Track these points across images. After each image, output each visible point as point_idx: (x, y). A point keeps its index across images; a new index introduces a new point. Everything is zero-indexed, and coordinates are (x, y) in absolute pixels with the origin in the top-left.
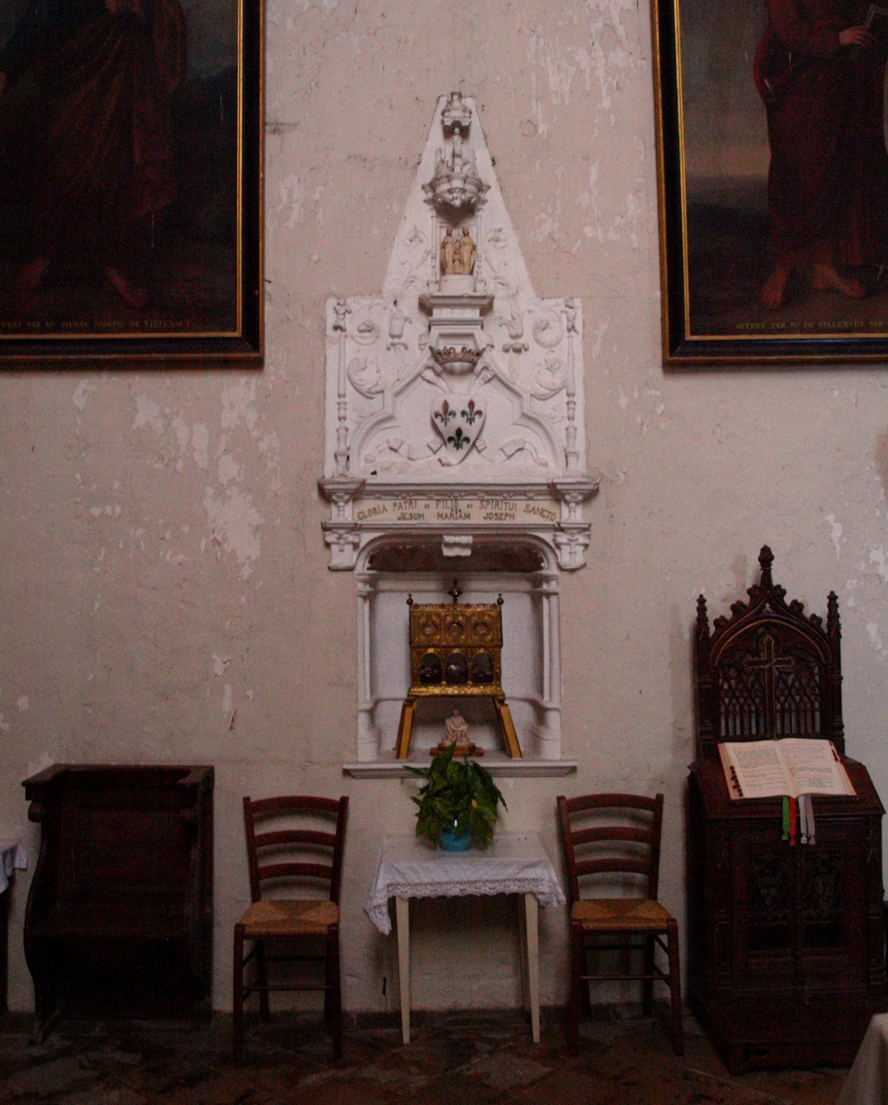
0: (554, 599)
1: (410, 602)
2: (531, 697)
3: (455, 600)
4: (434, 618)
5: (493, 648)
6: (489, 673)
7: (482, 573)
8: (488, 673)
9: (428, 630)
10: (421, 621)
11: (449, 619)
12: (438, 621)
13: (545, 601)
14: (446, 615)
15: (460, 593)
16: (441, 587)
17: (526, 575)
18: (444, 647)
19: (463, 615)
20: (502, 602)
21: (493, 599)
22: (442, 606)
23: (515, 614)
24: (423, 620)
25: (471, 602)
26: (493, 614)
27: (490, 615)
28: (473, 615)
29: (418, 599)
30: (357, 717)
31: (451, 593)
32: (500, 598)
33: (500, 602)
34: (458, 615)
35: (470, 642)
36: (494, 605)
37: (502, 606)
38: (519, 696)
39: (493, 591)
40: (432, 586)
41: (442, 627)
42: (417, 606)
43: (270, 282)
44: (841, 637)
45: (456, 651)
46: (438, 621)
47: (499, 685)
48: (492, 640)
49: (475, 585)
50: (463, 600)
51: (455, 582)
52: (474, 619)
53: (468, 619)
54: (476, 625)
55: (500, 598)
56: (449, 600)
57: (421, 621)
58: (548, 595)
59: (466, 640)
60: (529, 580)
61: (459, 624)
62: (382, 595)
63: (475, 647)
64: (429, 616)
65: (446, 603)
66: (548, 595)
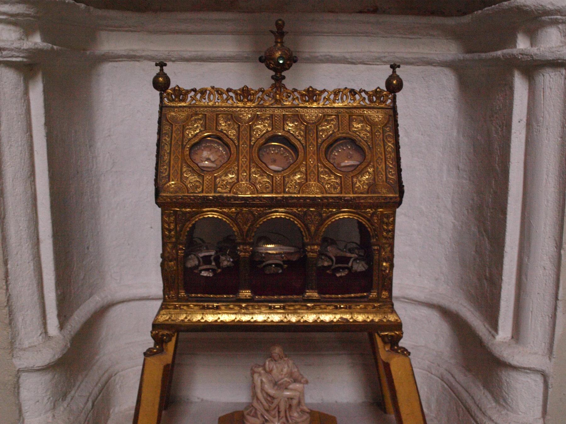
0: (551, 82)
1: (161, 84)
2: (445, 303)
3: (278, 79)
4: (223, 125)
5: (375, 206)
6: (356, 260)
7: (343, 17)
8: (360, 267)
9: (207, 158)
10: (190, 134)
11: (261, 127)
12: (232, 133)
13: (520, 86)
14: (256, 118)
15: (291, 60)
16: (246, 49)
17: (450, 22)
18: (246, 202)
19: (297, 118)
20: (400, 86)
21: (375, 78)
22: (245, 93)
23: (429, 121)
24: (194, 131)
25: (319, 87)
26: (377, 116)
27: (366, 120)
28: (324, 118)
29: (181, 77)
30: (17, 386)
31: (266, 60)
32: (394, 76)
33: (394, 86)
34: (285, 119)
35: (314, 192)
36: (377, 93)
37: (399, 95)
38: (422, 297)
39: (378, 60)
40: (227, 46)
41: (244, 147)
42: (180, 94)
43: (272, 32)
44: (397, 114)
45: (279, 214)
46: (232, 133)
47: (387, 304)
48: (372, 187)
49: (327, 46)
50: (298, 79)
51: (280, 33)
52: (328, 128)
53: (311, 128)
54: (333, 143)
55: (394, 76)
56: (258, 79)
57: (190, 134)
58: (532, 68)
59: (302, 186)
60: (455, 35)
61: (285, 140)
62: (107, 67)
63: (328, 206)
64: (210, 118)
65: (253, 86)
66: (532, 68)
